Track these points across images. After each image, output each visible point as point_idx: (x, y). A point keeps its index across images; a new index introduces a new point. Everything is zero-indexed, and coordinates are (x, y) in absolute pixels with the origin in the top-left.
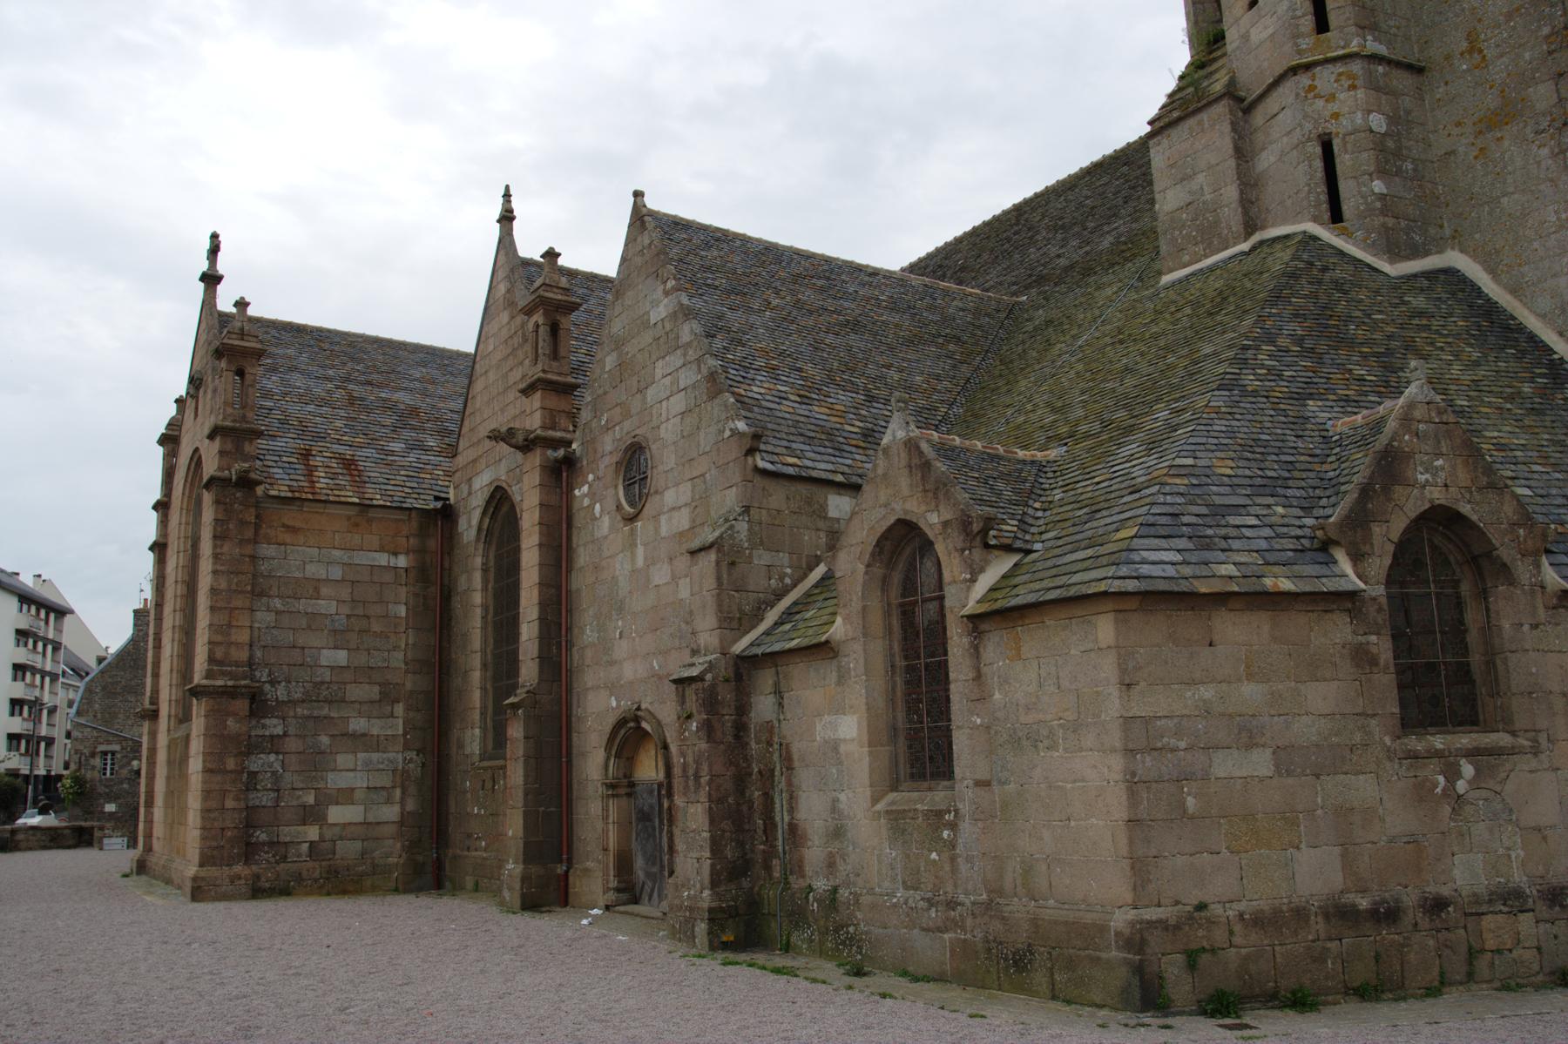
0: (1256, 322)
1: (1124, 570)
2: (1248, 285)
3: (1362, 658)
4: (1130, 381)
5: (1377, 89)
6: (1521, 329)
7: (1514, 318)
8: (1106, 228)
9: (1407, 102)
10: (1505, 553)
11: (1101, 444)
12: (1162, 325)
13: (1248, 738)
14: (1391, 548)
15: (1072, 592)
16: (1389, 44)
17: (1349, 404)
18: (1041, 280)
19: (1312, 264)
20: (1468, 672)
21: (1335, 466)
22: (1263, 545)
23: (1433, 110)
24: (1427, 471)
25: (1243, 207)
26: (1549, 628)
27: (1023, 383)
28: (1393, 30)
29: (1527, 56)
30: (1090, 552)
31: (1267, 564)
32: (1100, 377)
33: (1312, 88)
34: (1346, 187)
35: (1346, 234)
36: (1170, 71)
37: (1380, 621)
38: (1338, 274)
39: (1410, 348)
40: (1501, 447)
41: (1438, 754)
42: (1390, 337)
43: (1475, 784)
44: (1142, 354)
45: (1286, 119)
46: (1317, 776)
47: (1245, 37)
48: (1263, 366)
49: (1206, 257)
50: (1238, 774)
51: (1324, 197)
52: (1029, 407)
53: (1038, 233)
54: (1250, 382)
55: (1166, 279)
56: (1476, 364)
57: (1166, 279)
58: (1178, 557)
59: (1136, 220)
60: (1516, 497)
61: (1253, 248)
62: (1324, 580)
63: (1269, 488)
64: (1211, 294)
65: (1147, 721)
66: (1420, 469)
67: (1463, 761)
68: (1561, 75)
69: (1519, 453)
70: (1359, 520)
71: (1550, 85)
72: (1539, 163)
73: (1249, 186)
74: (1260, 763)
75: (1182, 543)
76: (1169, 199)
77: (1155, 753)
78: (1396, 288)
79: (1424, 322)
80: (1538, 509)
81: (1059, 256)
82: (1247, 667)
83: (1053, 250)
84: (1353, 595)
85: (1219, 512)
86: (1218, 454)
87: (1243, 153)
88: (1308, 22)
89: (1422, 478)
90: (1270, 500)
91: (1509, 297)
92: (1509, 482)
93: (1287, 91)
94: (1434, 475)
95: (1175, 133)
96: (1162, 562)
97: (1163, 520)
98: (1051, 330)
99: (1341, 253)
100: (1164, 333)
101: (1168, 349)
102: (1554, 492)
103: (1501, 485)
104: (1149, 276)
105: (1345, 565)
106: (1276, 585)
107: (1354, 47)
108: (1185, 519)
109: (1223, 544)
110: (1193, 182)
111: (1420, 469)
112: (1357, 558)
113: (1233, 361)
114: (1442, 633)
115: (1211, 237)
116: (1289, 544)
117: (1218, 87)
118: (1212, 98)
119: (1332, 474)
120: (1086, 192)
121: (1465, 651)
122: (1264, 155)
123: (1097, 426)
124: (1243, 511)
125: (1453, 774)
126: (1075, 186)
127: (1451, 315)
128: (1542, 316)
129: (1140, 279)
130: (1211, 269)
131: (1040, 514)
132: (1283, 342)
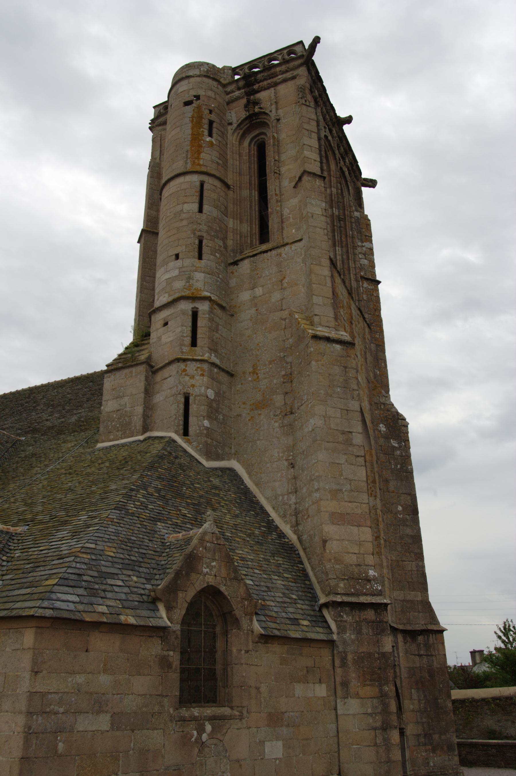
0: (140, 477)
1: (46, 604)
2: (139, 458)
3: (164, 663)
4: (70, 496)
5: (213, 379)
6: (258, 503)
7: (256, 497)
8: (75, 412)
9: (224, 388)
10: (238, 613)
11: (48, 528)
12: (93, 469)
13: (98, 706)
14: (186, 605)
15: (14, 613)
16: (221, 360)
17: (177, 527)
18: (35, 431)
19: (171, 453)
20: (215, 674)
21: (165, 558)
22: (123, 597)
23: (235, 394)
24: (208, 567)
25: (144, 418)
26: (253, 653)
27: (12, 485)
28: (223, 354)
29: (275, 381)
30: (28, 590)
31: (124, 607)
32: (55, 490)
33: (185, 370)
34: (192, 420)
35: (189, 442)
36: (122, 343)
37: (176, 644)
38: (182, 461)
39: (209, 503)
40: (243, 559)
41: (195, 719)
42: (201, 497)
43: (211, 736)
44: (80, 483)
45: (171, 381)
46: (133, 731)
47: (160, 338)
48: (139, 501)
49: (122, 438)
50: (90, 728)
51: (182, 423)
52: (12, 500)
53: (38, 405)
54: (131, 507)
55: (100, 445)
56: (237, 516)
57: (100, 445)
58: (77, 599)
59: (91, 411)
60: (246, 585)
61: (145, 440)
62: (151, 619)
63: (131, 566)
64: (120, 458)
65: (43, 695)
66: (205, 566)
67: (207, 723)
68: (286, 393)
69: (250, 563)
70: (173, 589)
71: (282, 396)
72: (274, 429)
73: (149, 408)
74: (103, 722)
75: (81, 591)
76: (109, 406)
77: (45, 715)
78: (207, 473)
79: (217, 492)
80: (255, 592)
81: (47, 420)
82: (105, 665)
83: (45, 416)
84: (164, 629)
85: (104, 576)
86: (109, 544)
87: (149, 392)
88: (188, 340)
89: (205, 570)
90: (131, 573)
91: (254, 487)
92: (244, 577)
93: (173, 369)
94: (211, 570)
95: (118, 374)
96: (68, 601)
97: (73, 577)
98: (34, 459)
99: (185, 451)
100: (93, 474)
101: (94, 483)
102: (262, 584)
103: (240, 578)
104: (91, 441)
105: (163, 612)
106: (126, 620)
107: (206, 357)
108: (85, 578)
109: (102, 594)
110: (121, 399)
111: (205, 566)
112: (169, 609)
113: (124, 496)
114: (205, 652)
115: (125, 429)
116: (136, 598)
117: (143, 358)
118: (138, 362)
119: (163, 562)
120: (68, 390)
121: (215, 662)
122: (158, 395)
123: (48, 518)
124: (116, 577)
125: (201, 730)
126: (64, 386)
127: (229, 491)
128: (267, 498)
129: (87, 442)
130: (123, 445)
131: (5, 563)
132: (151, 490)
